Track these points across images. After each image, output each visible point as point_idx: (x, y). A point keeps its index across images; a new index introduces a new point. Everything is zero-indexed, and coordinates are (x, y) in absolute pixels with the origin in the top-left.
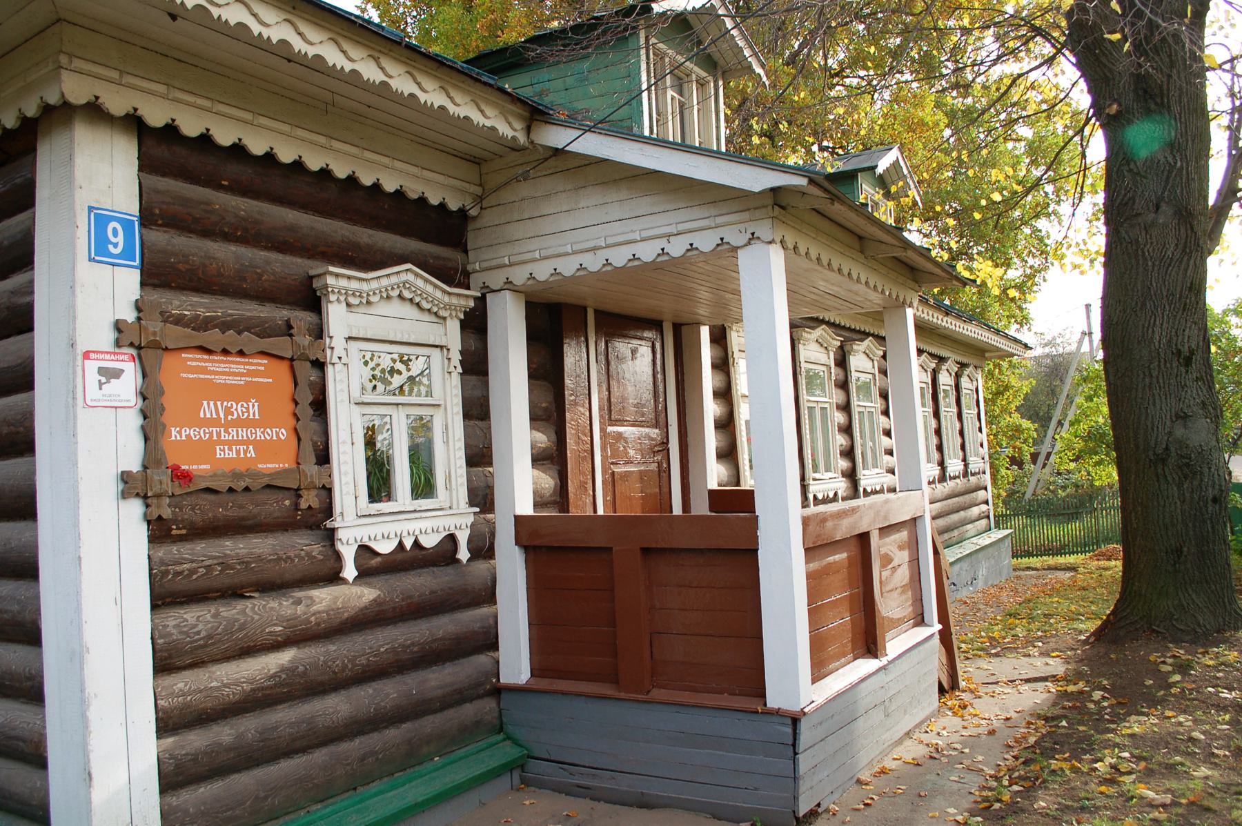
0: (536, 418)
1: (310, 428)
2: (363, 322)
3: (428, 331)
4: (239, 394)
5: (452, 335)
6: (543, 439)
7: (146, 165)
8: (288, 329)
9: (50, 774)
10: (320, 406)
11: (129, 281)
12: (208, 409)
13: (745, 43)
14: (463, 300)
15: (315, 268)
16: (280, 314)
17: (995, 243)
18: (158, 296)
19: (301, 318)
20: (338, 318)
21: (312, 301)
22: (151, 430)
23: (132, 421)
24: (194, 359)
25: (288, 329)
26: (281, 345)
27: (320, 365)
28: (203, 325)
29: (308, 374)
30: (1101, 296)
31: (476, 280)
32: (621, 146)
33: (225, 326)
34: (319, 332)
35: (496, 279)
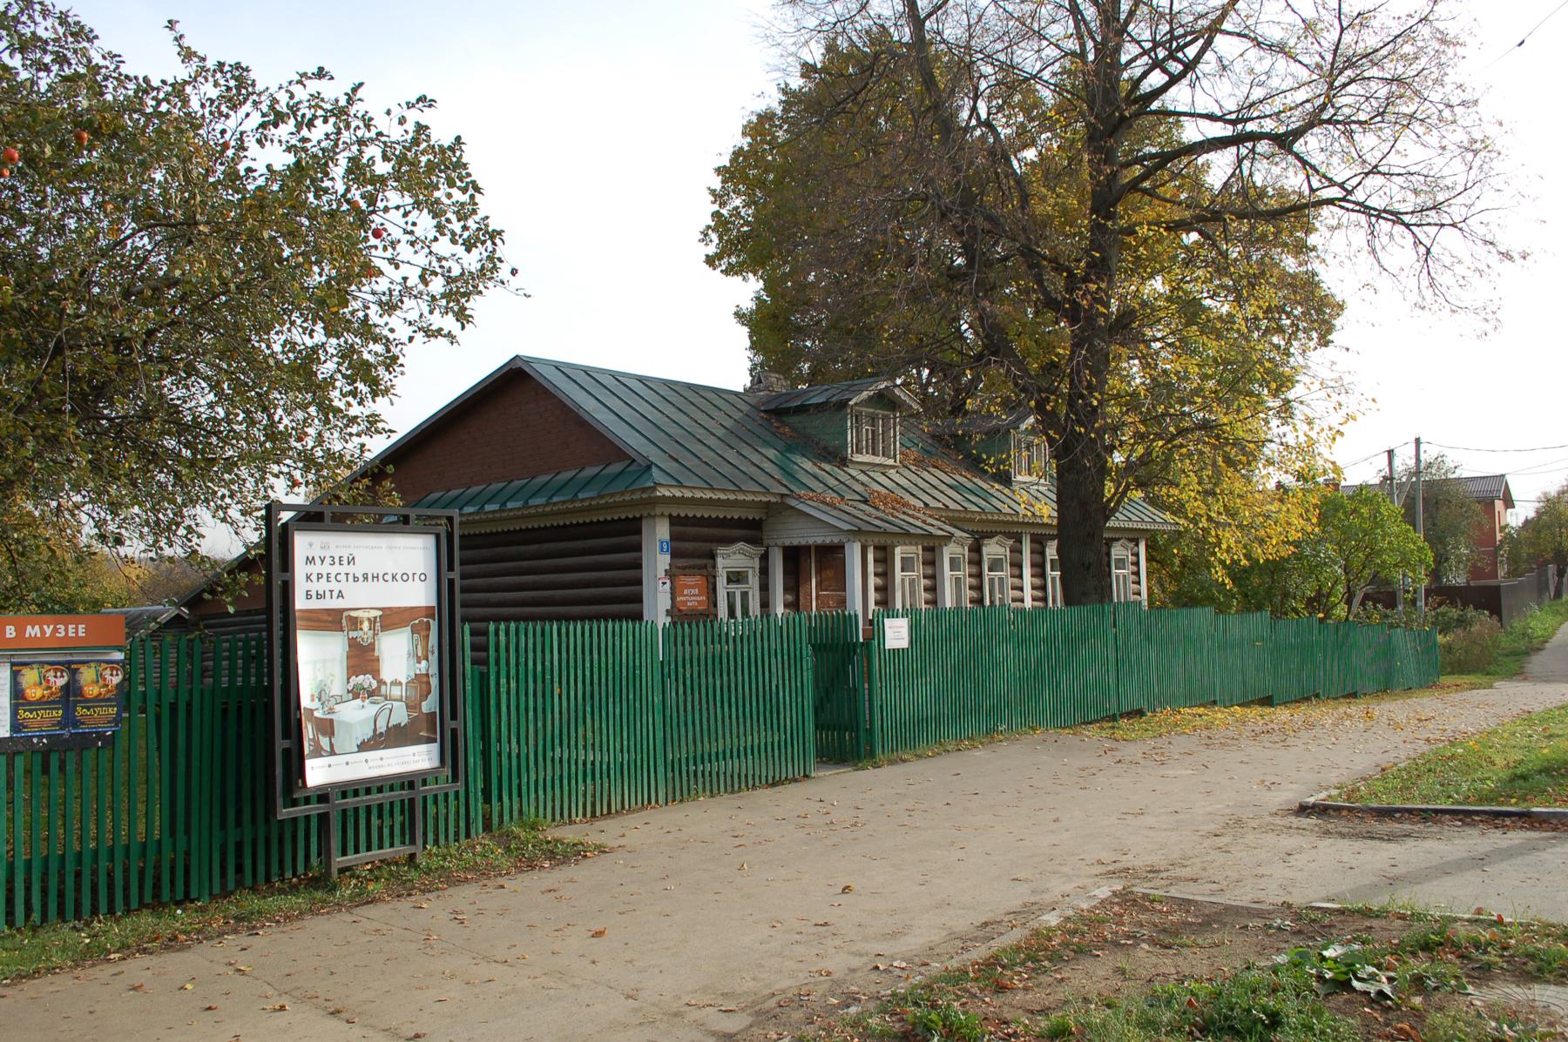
0: (786, 590)
1: (712, 596)
2: (728, 562)
3: (748, 562)
4: (693, 587)
5: (756, 563)
6: (790, 598)
7: (671, 524)
8: (705, 567)
9: (792, 798)
10: (715, 589)
11: (667, 558)
12: (686, 592)
13: (1453, 604)
14: (762, 550)
15: (713, 546)
16: (704, 561)
17: (800, 378)
18: (675, 561)
19: (709, 562)
20: (720, 561)
21: (713, 557)
22: (673, 599)
23: (669, 596)
24: (682, 578)
25: (705, 567)
26: (704, 572)
27: (715, 577)
28: (685, 568)
29: (712, 580)
30: (748, 343)
31: (765, 543)
32: (1342, 709)
33: (690, 567)
34: (714, 566)
35: (772, 543)
